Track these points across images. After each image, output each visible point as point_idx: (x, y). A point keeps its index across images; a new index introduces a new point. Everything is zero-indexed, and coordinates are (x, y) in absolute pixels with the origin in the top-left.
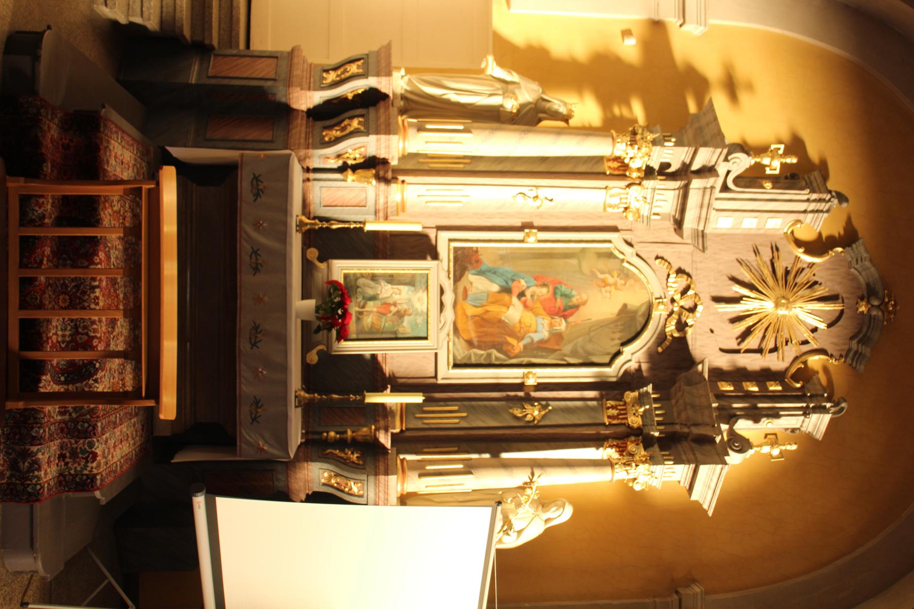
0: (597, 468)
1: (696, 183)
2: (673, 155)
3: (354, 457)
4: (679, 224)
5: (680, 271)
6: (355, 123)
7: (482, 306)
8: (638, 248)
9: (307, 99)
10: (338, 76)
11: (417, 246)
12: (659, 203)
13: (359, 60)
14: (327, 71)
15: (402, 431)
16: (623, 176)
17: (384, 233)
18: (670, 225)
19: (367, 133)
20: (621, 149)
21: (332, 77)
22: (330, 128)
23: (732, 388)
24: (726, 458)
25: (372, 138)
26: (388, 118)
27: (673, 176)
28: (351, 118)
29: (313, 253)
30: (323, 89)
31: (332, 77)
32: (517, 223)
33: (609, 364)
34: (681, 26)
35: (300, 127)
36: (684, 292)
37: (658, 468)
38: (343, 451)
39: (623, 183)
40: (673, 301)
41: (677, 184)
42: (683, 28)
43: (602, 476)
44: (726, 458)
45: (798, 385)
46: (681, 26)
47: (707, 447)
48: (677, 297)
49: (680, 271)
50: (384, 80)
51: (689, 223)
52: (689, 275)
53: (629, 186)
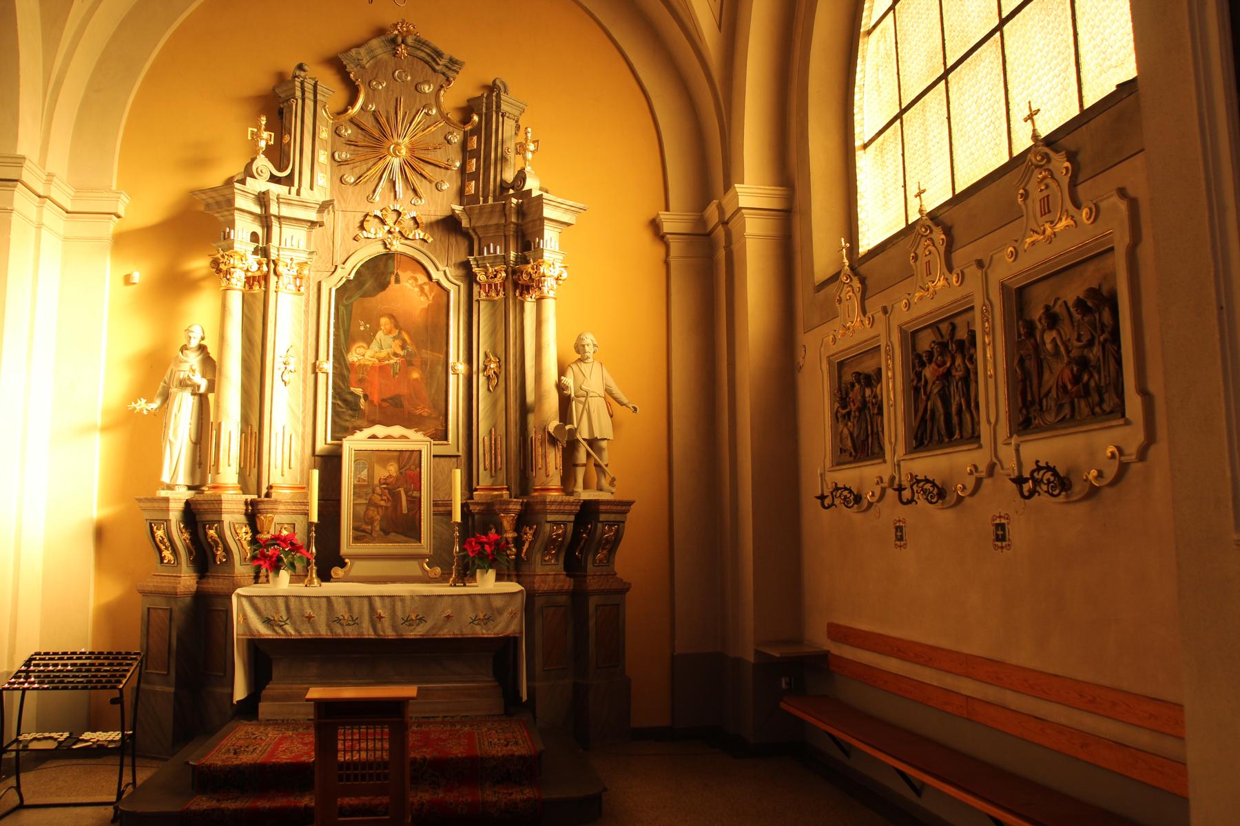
0: (100, 761)
1: (274, 209)
2: (244, 229)
3: (212, 532)
4: (313, 224)
5: (362, 227)
6: (212, 532)
7: (309, 563)
8: (338, 261)
9: (187, 580)
10: (167, 548)
11: (329, 464)
12: (295, 243)
13: (151, 528)
14: (162, 559)
15: (508, 489)
16: (266, 278)
17: (319, 505)
18: (317, 229)
19: (220, 522)
20: (238, 279)
21: (167, 554)
22: (215, 556)
23: (473, 183)
24: (534, 195)
25: (226, 518)
26: (206, 502)
27: (267, 227)
28: (206, 534)
29: (337, 572)
30: (179, 563)
31: (167, 554)
32: (311, 377)
33: (448, 292)
34: (119, 217)
35: (213, 585)
36: (383, 222)
37: (546, 255)
38: (524, 543)
39: (273, 279)
40: (390, 232)
41: (275, 225)
42: (121, 213)
43: (550, 307)
44: (534, 195)
45: (476, 118)
46: (119, 217)
47: (525, 207)
48: (387, 228)
49: (362, 227)
50: (172, 505)
51: (312, 215)
52: (367, 215)
53: (275, 273)
